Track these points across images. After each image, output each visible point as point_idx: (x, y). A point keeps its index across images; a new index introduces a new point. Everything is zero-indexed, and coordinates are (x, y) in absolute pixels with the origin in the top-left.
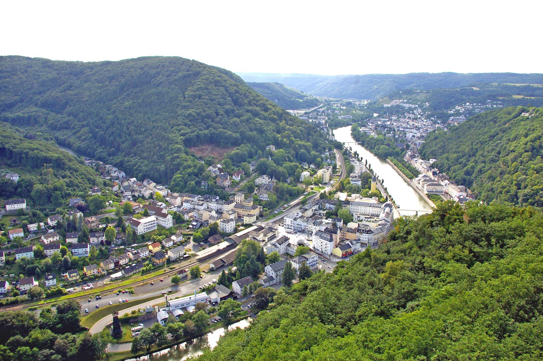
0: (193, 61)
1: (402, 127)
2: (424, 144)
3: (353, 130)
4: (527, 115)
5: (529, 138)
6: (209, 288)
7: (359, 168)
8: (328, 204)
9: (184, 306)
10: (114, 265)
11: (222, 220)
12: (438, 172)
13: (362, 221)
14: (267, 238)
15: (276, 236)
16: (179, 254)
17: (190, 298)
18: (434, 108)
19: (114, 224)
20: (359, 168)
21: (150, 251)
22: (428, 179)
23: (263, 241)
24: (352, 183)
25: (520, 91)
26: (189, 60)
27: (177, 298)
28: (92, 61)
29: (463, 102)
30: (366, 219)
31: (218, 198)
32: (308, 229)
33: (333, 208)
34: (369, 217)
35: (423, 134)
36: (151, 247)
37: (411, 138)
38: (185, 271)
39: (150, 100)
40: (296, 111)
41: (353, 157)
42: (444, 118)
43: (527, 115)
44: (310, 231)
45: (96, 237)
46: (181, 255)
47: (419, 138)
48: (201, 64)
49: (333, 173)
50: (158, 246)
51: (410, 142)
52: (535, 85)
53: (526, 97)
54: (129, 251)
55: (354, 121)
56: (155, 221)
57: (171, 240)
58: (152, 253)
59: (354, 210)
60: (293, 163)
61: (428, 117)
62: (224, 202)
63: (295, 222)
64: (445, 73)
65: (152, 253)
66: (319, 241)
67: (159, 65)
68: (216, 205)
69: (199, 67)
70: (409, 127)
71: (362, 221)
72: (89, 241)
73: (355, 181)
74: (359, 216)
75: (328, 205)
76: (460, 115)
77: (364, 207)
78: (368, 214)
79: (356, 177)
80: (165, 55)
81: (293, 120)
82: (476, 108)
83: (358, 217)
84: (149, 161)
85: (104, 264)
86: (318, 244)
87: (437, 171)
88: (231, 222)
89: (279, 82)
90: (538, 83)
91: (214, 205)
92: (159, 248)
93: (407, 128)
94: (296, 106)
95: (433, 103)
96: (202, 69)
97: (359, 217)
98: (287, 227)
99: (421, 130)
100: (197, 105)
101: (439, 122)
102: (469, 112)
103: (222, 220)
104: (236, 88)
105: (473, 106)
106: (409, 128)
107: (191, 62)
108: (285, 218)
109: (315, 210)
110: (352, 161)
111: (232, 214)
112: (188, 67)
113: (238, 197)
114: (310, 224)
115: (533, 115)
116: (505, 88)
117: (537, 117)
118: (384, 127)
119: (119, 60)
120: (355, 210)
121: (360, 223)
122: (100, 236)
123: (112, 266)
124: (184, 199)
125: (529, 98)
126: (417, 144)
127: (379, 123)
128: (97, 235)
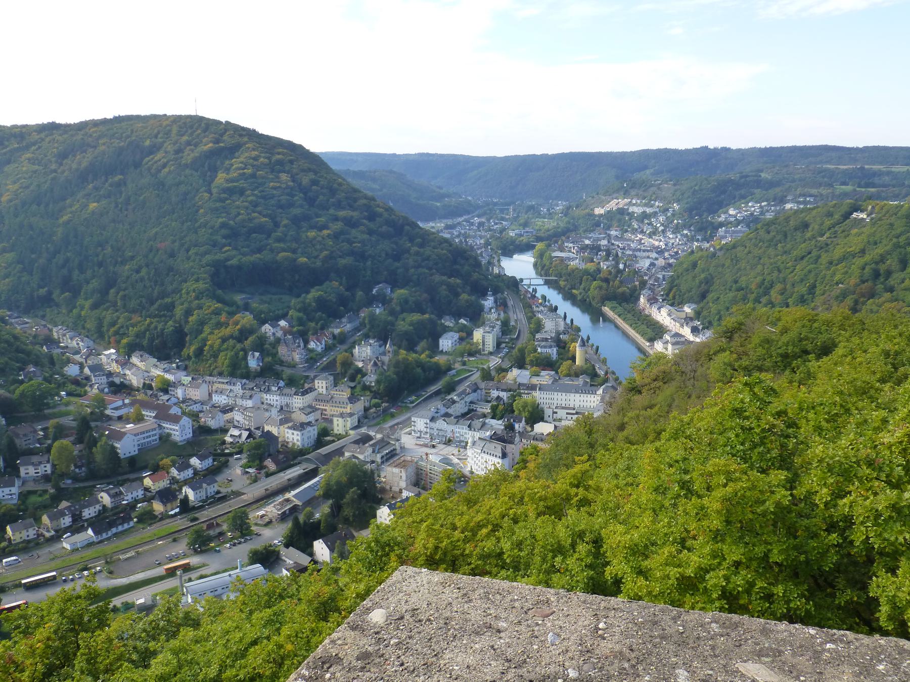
0: (228, 123)
1: (630, 250)
2: (672, 276)
3: (540, 256)
4: (863, 216)
5: (867, 258)
6: (91, 494)
7: (550, 326)
8: (495, 391)
9: (217, 593)
10: (70, 520)
11: (290, 424)
12: (700, 327)
13: (560, 420)
14: (379, 456)
15: (398, 452)
16: (206, 493)
17: (230, 575)
18: (690, 211)
19: (72, 438)
20: (550, 326)
21: (147, 489)
22: (683, 339)
23: (373, 462)
24: (539, 350)
25: (848, 176)
26: (220, 123)
27: (202, 577)
28: (20, 122)
29: (743, 201)
30: (569, 417)
31: (282, 383)
32: (457, 437)
33: (505, 398)
34: (574, 412)
35: (671, 261)
36: (147, 482)
37: (648, 269)
38: (218, 525)
39: (142, 198)
40: (432, 224)
41: (541, 304)
42: (708, 230)
43: (863, 216)
44: (463, 441)
45: (33, 464)
46: (209, 495)
47: (663, 268)
48: (243, 129)
49: (502, 335)
50: (162, 478)
51: (646, 274)
52: (876, 167)
53: (858, 189)
54: (103, 491)
55: (539, 239)
56: (155, 429)
57: (188, 466)
58: (150, 492)
59: (545, 401)
60: (427, 316)
61: (676, 230)
62: (293, 392)
63: (433, 425)
64: (705, 149)
65: (150, 492)
66: (480, 458)
67: (158, 133)
68: (278, 398)
69: (241, 135)
70: (643, 248)
71: (560, 420)
72: (19, 472)
73: (545, 347)
74: (555, 410)
75: (495, 394)
76: (738, 225)
77: (564, 394)
78: (572, 406)
79: (546, 340)
80: (170, 112)
81: (426, 238)
82: (768, 211)
83: (555, 413)
84: (141, 316)
85: (49, 517)
86: (479, 464)
87: (699, 325)
88: (309, 429)
89: (395, 170)
90: (881, 163)
91: (273, 399)
92: (165, 483)
93: (640, 250)
94: (432, 216)
95: (687, 203)
96: (246, 139)
97: (556, 413)
98: (418, 435)
99: (666, 254)
100: (238, 207)
101: (700, 237)
102: (752, 221)
103: (290, 424)
104: (312, 176)
105: (761, 207)
106: (644, 251)
107: (222, 126)
108: (413, 419)
109: (471, 402)
110: (538, 312)
111: (311, 413)
112: (217, 136)
113: (320, 382)
114: (463, 429)
115: (873, 216)
116: (820, 172)
117: (880, 219)
118: (596, 249)
119: (77, 121)
120: (548, 401)
121: (557, 424)
122: (40, 463)
123: (67, 521)
124: (214, 388)
125: (863, 190)
126: (659, 278)
127: (587, 242)
128: (35, 459)
